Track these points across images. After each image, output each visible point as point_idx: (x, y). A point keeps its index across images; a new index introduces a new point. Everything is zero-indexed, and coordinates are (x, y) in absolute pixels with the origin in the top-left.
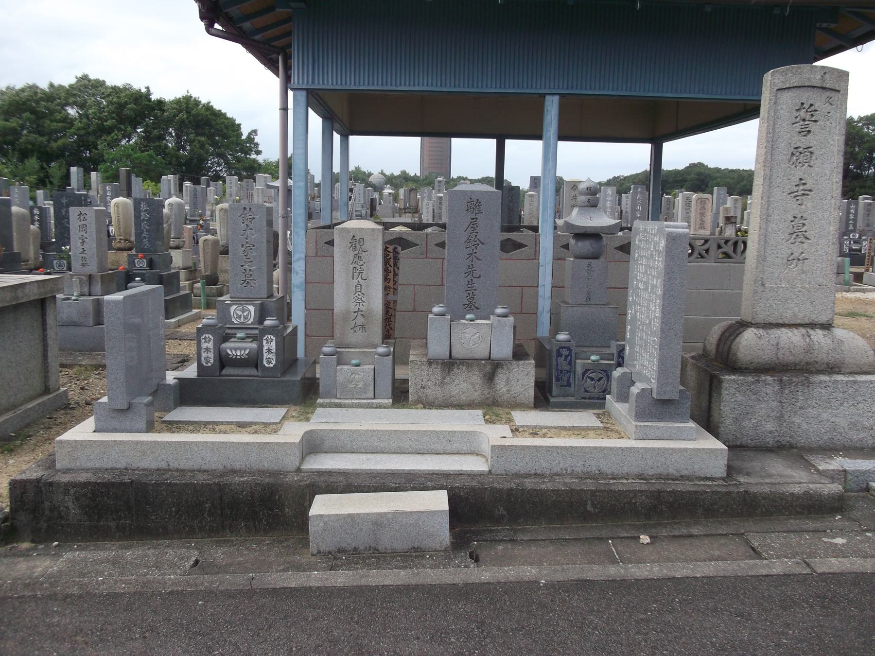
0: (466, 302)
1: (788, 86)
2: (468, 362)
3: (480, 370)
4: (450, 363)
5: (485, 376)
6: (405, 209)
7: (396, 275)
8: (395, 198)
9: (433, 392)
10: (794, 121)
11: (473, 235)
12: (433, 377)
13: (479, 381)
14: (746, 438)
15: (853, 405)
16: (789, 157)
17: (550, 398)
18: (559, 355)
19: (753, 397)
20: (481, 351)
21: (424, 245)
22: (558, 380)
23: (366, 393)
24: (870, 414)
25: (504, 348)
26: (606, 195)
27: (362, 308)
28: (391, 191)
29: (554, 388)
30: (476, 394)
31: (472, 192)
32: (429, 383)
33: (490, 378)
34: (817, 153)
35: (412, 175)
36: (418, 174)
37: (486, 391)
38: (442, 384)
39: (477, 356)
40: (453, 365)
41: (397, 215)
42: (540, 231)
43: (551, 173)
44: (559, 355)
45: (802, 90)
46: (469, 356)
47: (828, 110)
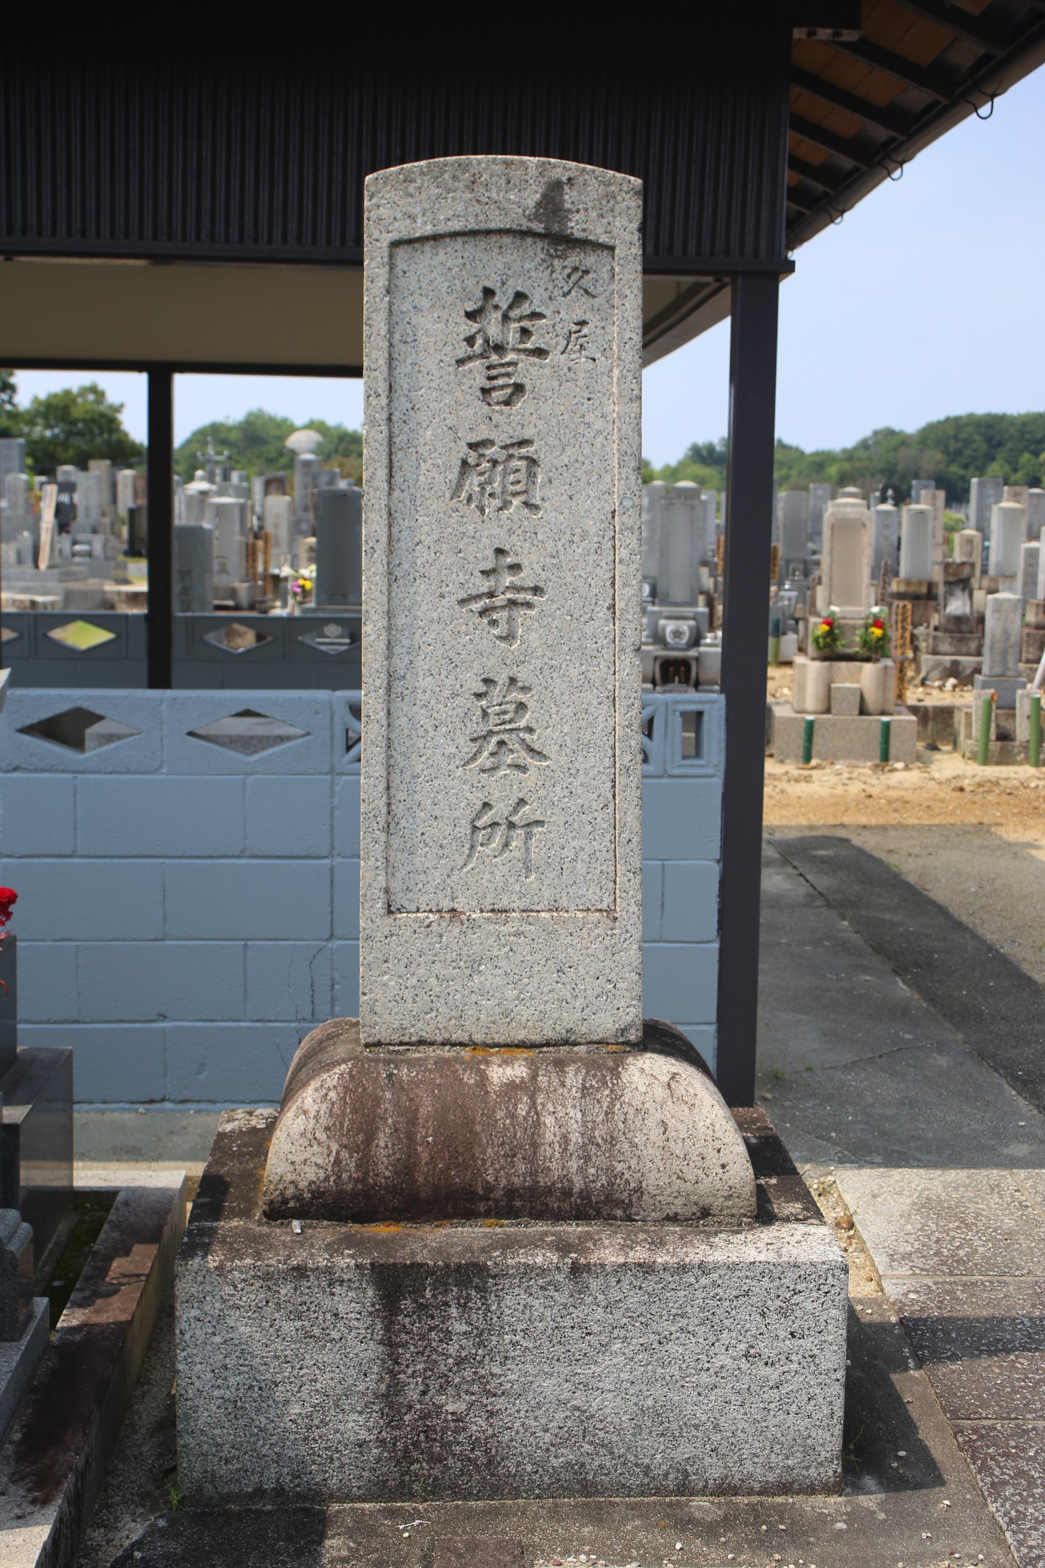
1: (428, 230)
10: (463, 350)
14: (273, 1469)
15: (645, 1348)
16: (453, 475)
19: (289, 1327)
24: (705, 1379)
34: (548, 460)
45: (482, 243)
47: (578, 314)
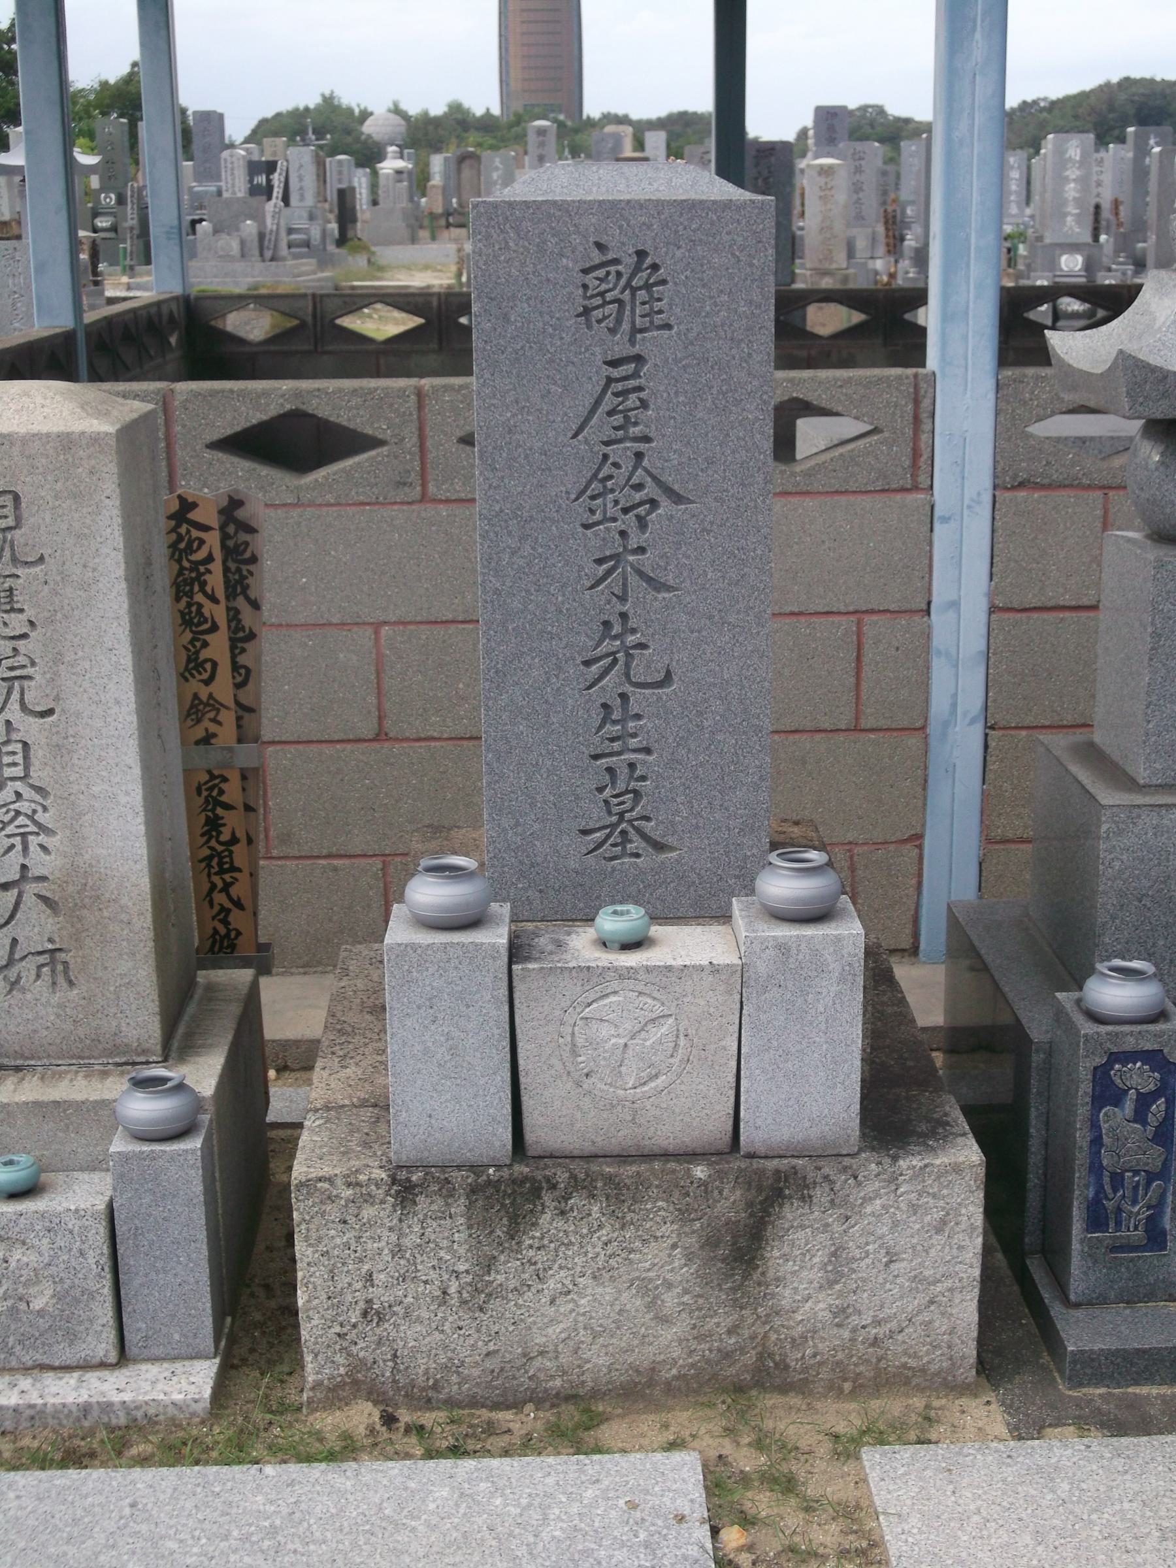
0: (596, 815)
2: (613, 1175)
3: (684, 1215)
4: (517, 1186)
5: (711, 1243)
6: (447, 214)
7: (242, 638)
8: (419, 181)
9: (431, 1338)
11: (622, 453)
12: (424, 1268)
13: (680, 1271)
17: (1056, 1310)
18: (1106, 1092)
20: (687, 1109)
21: (411, 442)
22: (1097, 1219)
23: (72, 1337)
25: (812, 1088)
26: (1062, 162)
27: (40, 863)
28: (400, 164)
29: (1076, 1264)
30: (667, 1335)
31: (611, 209)
32: (408, 1292)
33: (741, 1251)
35: (479, 111)
36: (496, 111)
37: (722, 1320)
38: (480, 1295)
39: (667, 1133)
40: (536, 1193)
41: (424, 234)
42: (933, 359)
43: (983, 88)
44: (1106, 1092)
46: (622, 1136)
